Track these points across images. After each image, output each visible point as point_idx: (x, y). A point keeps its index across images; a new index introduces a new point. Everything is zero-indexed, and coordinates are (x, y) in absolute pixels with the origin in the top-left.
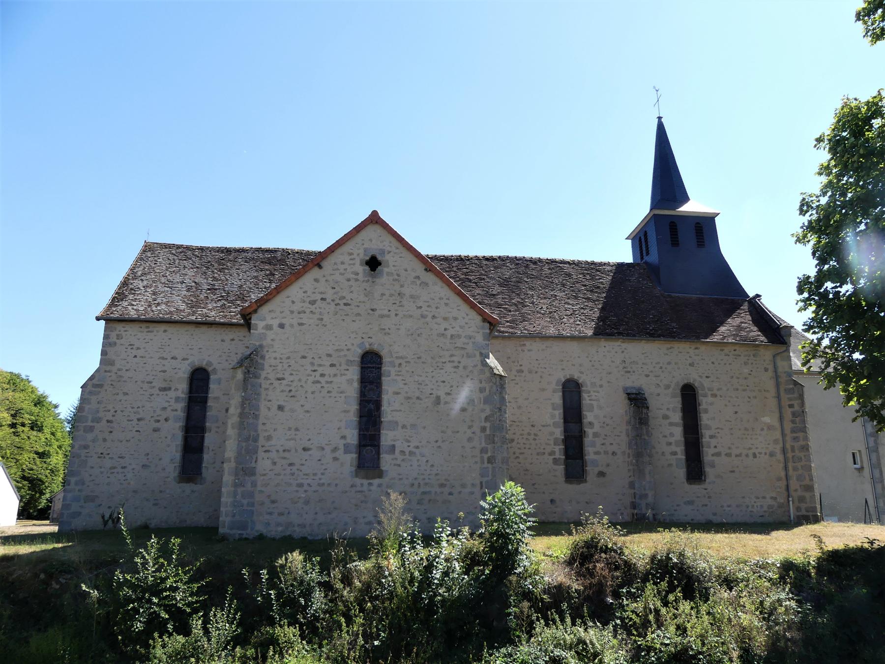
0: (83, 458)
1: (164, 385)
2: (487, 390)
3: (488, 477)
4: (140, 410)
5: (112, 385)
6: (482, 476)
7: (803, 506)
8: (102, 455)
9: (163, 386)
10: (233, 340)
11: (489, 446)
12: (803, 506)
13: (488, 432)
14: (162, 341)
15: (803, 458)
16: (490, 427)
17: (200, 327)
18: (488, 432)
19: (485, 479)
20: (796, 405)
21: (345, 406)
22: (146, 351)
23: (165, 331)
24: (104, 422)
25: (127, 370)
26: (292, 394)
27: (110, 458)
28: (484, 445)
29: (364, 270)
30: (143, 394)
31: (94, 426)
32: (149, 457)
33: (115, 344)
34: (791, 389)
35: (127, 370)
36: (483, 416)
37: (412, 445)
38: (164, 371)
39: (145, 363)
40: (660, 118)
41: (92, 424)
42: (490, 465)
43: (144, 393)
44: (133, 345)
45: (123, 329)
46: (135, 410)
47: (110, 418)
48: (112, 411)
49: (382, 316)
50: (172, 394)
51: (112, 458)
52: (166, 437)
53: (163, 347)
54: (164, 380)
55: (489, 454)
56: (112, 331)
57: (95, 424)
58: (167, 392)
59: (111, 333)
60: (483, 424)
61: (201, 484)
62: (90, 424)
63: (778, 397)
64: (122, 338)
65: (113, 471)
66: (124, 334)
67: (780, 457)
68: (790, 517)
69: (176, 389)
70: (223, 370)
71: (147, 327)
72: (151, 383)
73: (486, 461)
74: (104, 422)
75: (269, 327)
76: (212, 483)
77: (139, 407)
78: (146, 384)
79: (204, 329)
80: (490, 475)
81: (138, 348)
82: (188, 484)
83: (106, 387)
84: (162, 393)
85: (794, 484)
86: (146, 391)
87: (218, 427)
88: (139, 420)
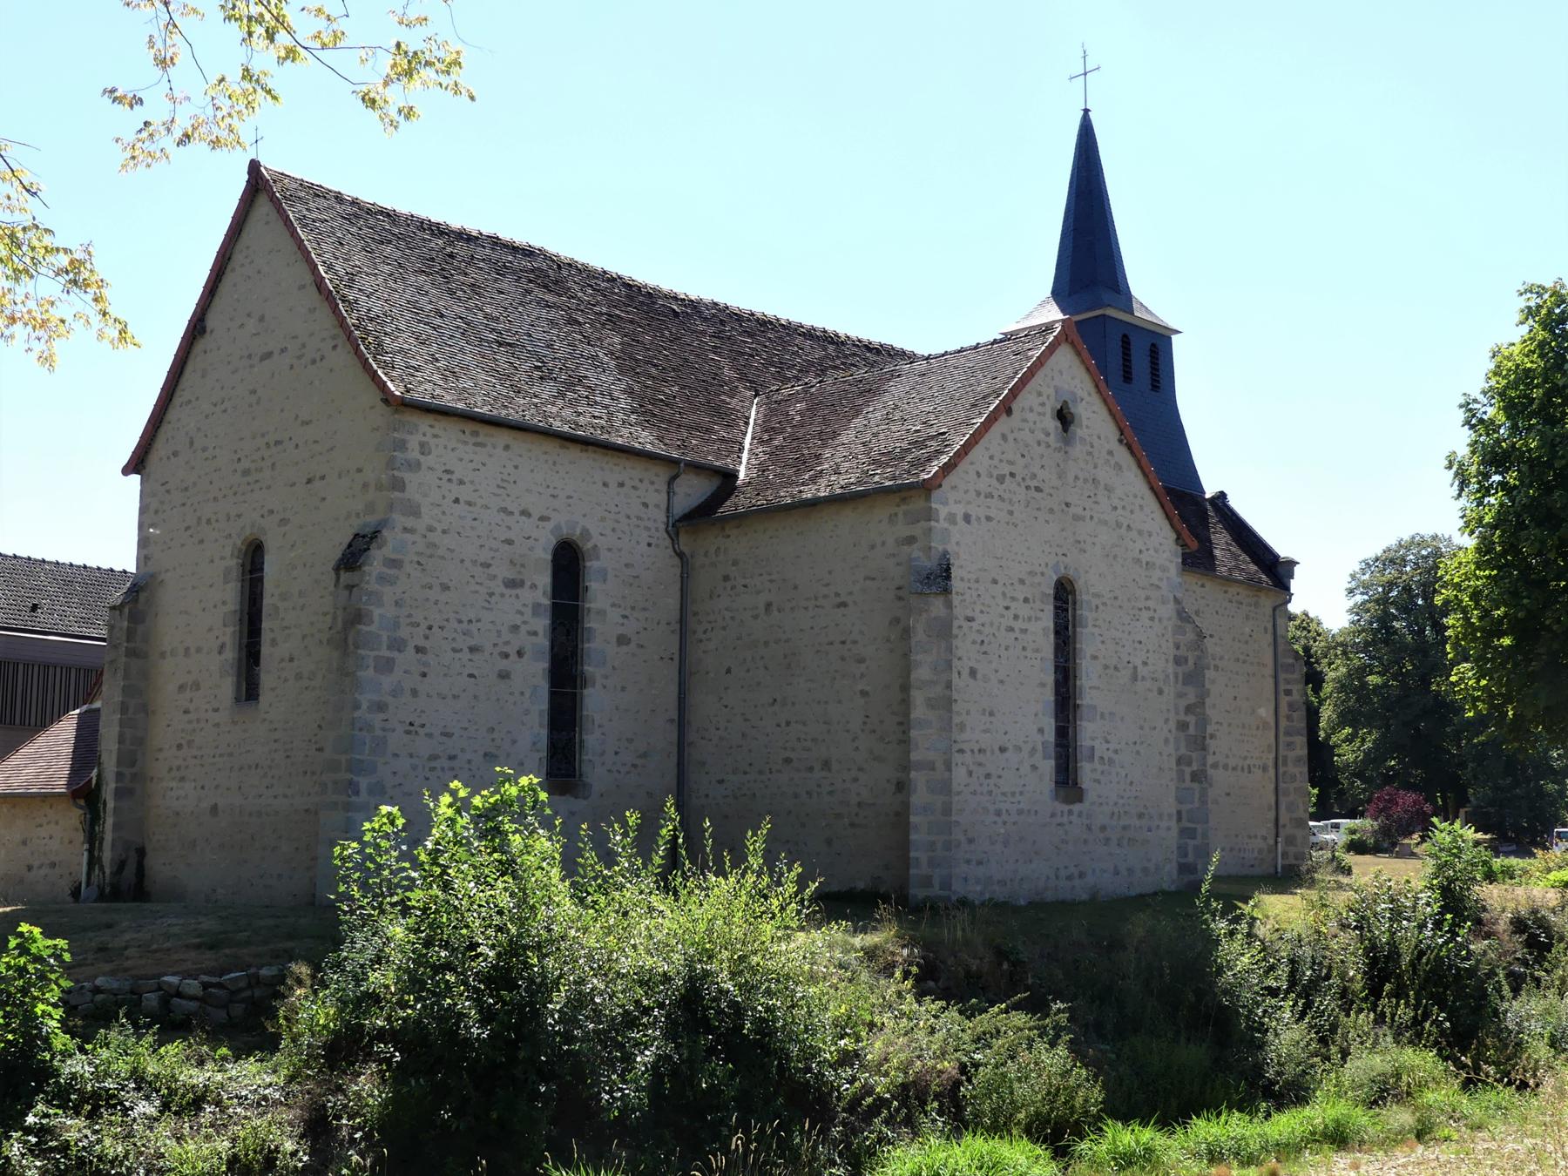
0: (378, 733)
1: (510, 575)
2: (1191, 662)
3: (1192, 802)
4: (473, 628)
5: (419, 563)
6: (1180, 800)
7: (1292, 850)
8: (412, 728)
9: (511, 577)
10: (621, 485)
11: (1194, 755)
12: (1292, 850)
13: (1192, 730)
14: (503, 470)
15: (1298, 775)
16: (1196, 723)
17: (568, 448)
18: (1192, 730)
19: (1185, 807)
20: (1294, 692)
21: (1042, 675)
22: (476, 491)
23: (507, 448)
24: (410, 650)
25: (444, 532)
26: (984, 648)
27: (426, 735)
28: (1183, 751)
29: (1056, 427)
30: (477, 592)
31: (393, 659)
32: (495, 735)
33: (418, 464)
34: (1290, 665)
35: (444, 532)
36: (1183, 703)
37: (1112, 746)
38: (509, 542)
39: (475, 519)
40: (1086, 111)
41: (387, 654)
42: (1195, 785)
43: (478, 588)
44: (452, 473)
45: (430, 431)
46: (465, 625)
47: (422, 643)
48: (424, 625)
49: (1077, 518)
50: (527, 595)
51: (429, 735)
52: (522, 693)
53: (504, 485)
54: (511, 561)
55: (1195, 768)
56: (412, 433)
57: (395, 654)
58: (518, 591)
59: (408, 437)
60: (1182, 717)
61: (585, 798)
62: (385, 653)
63: (1276, 677)
64: (429, 453)
65: (433, 764)
66: (433, 442)
67: (1272, 772)
68: (1276, 868)
69: (534, 586)
70: (610, 550)
71: (475, 434)
72: (489, 566)
73: (1188, 777)
74: (410, 650)
75: (952, 519)
76: (602, 795)
77: (470, 621)
78: (480, 569)
79: (574, 452)
80: (1196, 800)
81: (461, 482)
82: (563, 798)
83: (408, 568)
84: (507, 592)
85: (1284, 818)
86: (481, 584)
87: (606, 677)
88: (472, 649)
